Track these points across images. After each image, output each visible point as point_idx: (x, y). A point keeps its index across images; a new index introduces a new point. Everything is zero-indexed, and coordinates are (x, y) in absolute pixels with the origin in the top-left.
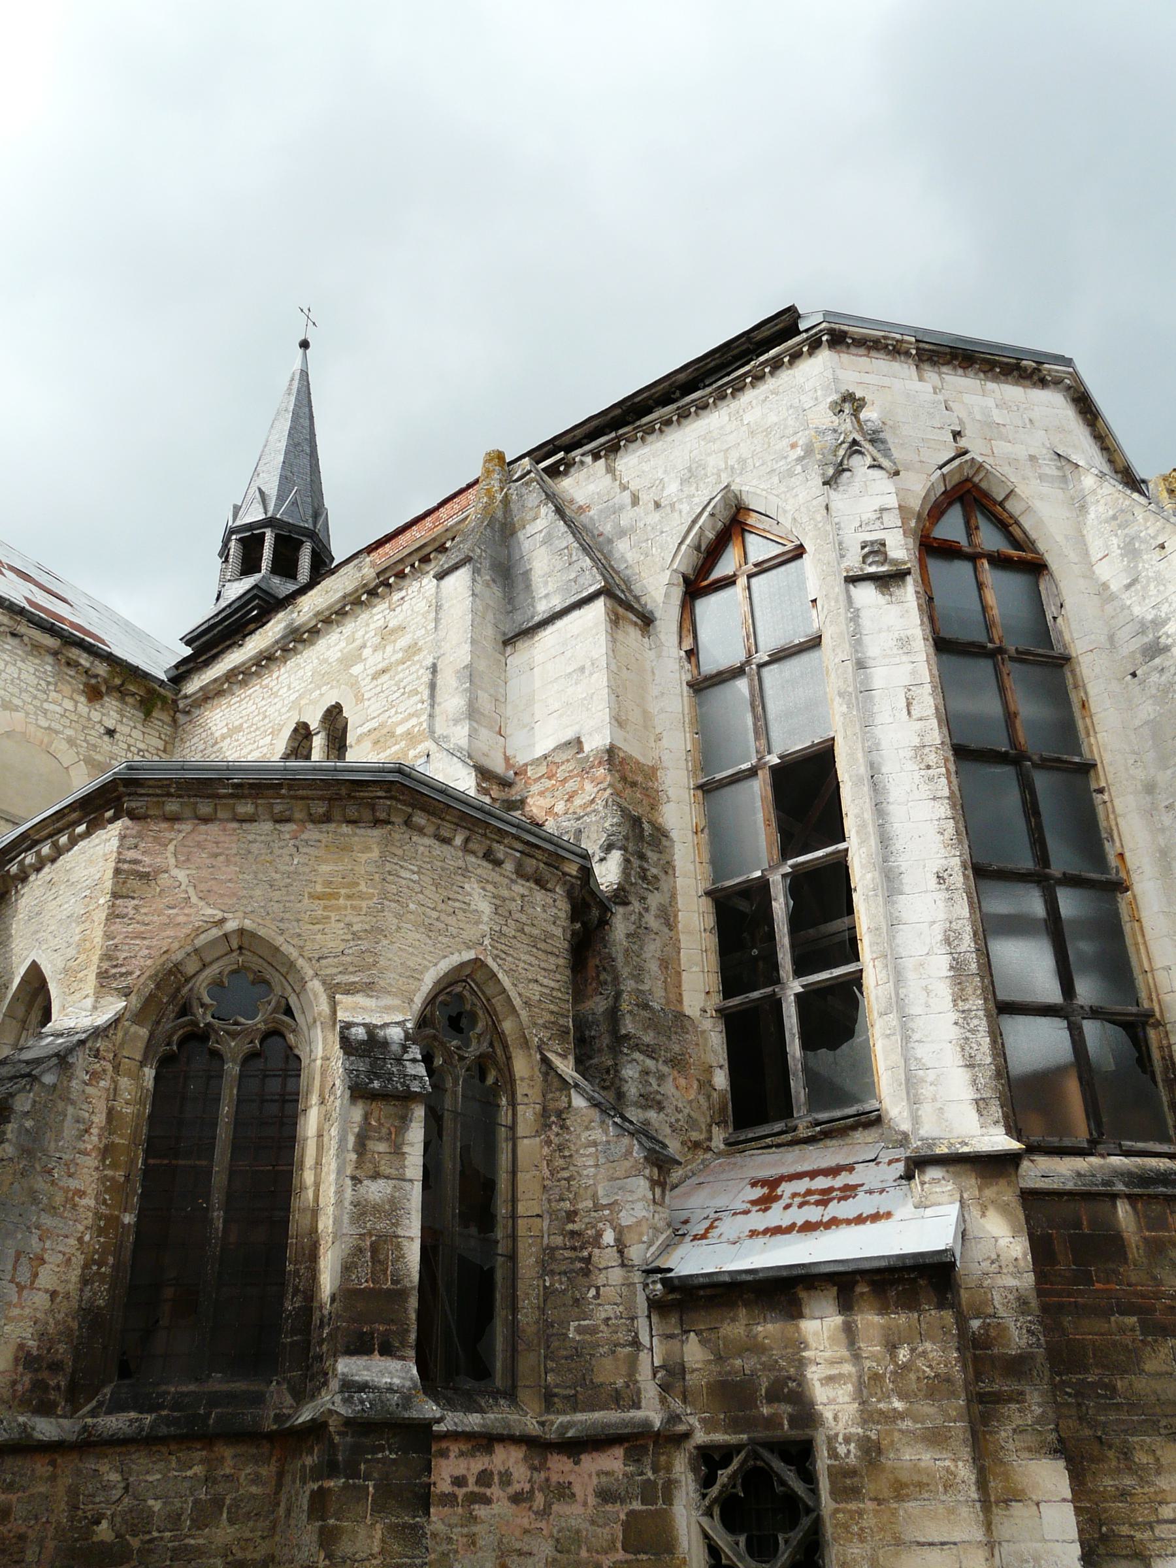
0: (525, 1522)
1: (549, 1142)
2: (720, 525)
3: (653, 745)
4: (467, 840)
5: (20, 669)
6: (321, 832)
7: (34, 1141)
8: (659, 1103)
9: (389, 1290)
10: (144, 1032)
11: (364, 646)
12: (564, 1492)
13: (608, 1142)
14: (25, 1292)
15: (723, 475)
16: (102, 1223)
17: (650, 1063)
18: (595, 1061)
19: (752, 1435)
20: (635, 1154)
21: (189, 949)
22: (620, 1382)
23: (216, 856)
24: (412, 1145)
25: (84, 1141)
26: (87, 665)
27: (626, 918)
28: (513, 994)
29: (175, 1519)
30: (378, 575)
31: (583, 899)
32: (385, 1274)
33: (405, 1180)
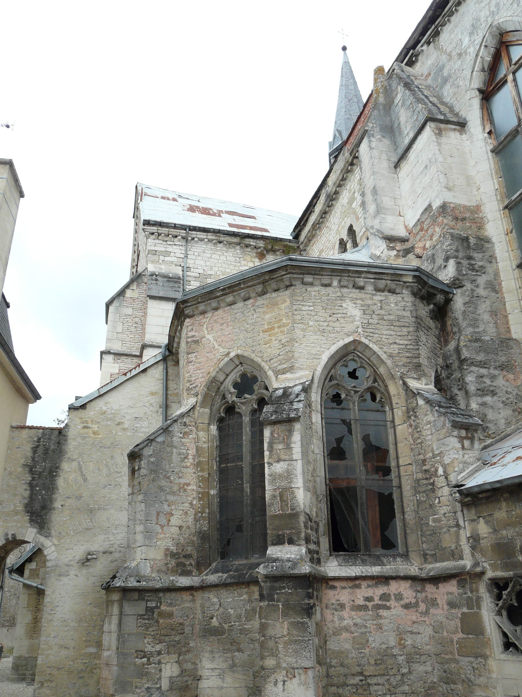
0: (414, 618)
1: (411, 426)
2: (492, 50)
3: (476, 193)
4: (340, 281)
5: (226, 256)
6: (264, 300)
7: (157, 466)
8: (493, 391)
9: (290, 514)
10: (207, 410)
11: (355, 192)
12: (433, 603)
13: (435, 420)
14: (165, 528)
15: (489, 19)
16: (200, 496)
17: (483, 371)
18: (453, 376)
19: (515, 572)
20: (447, 425)
21: (217, 369)
22: (453, 546)
23: (223, 324)
24: (295, 443)
25: (185, 462)
26: (254, 244)
27: (463, 294)
28: (380, 353)
29: (239, 617)
30: (351, 154)
31: (428, 292)
32: (287, 506)
33: (293, 460)
